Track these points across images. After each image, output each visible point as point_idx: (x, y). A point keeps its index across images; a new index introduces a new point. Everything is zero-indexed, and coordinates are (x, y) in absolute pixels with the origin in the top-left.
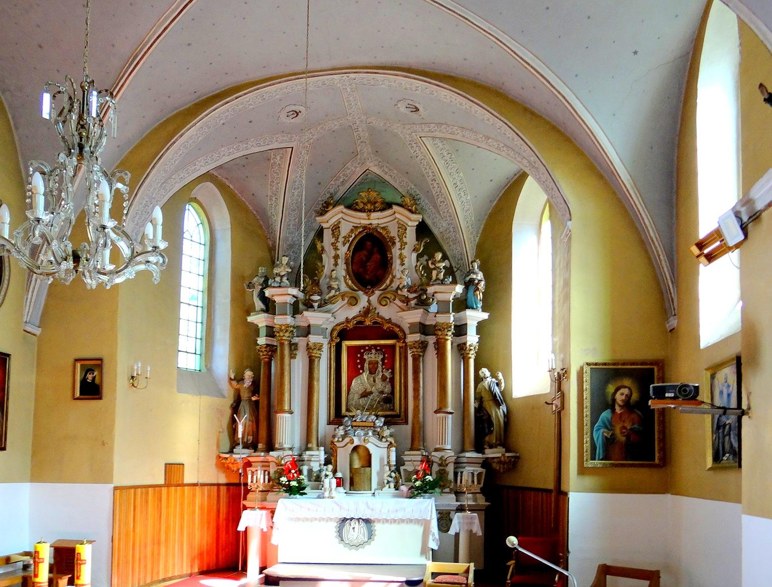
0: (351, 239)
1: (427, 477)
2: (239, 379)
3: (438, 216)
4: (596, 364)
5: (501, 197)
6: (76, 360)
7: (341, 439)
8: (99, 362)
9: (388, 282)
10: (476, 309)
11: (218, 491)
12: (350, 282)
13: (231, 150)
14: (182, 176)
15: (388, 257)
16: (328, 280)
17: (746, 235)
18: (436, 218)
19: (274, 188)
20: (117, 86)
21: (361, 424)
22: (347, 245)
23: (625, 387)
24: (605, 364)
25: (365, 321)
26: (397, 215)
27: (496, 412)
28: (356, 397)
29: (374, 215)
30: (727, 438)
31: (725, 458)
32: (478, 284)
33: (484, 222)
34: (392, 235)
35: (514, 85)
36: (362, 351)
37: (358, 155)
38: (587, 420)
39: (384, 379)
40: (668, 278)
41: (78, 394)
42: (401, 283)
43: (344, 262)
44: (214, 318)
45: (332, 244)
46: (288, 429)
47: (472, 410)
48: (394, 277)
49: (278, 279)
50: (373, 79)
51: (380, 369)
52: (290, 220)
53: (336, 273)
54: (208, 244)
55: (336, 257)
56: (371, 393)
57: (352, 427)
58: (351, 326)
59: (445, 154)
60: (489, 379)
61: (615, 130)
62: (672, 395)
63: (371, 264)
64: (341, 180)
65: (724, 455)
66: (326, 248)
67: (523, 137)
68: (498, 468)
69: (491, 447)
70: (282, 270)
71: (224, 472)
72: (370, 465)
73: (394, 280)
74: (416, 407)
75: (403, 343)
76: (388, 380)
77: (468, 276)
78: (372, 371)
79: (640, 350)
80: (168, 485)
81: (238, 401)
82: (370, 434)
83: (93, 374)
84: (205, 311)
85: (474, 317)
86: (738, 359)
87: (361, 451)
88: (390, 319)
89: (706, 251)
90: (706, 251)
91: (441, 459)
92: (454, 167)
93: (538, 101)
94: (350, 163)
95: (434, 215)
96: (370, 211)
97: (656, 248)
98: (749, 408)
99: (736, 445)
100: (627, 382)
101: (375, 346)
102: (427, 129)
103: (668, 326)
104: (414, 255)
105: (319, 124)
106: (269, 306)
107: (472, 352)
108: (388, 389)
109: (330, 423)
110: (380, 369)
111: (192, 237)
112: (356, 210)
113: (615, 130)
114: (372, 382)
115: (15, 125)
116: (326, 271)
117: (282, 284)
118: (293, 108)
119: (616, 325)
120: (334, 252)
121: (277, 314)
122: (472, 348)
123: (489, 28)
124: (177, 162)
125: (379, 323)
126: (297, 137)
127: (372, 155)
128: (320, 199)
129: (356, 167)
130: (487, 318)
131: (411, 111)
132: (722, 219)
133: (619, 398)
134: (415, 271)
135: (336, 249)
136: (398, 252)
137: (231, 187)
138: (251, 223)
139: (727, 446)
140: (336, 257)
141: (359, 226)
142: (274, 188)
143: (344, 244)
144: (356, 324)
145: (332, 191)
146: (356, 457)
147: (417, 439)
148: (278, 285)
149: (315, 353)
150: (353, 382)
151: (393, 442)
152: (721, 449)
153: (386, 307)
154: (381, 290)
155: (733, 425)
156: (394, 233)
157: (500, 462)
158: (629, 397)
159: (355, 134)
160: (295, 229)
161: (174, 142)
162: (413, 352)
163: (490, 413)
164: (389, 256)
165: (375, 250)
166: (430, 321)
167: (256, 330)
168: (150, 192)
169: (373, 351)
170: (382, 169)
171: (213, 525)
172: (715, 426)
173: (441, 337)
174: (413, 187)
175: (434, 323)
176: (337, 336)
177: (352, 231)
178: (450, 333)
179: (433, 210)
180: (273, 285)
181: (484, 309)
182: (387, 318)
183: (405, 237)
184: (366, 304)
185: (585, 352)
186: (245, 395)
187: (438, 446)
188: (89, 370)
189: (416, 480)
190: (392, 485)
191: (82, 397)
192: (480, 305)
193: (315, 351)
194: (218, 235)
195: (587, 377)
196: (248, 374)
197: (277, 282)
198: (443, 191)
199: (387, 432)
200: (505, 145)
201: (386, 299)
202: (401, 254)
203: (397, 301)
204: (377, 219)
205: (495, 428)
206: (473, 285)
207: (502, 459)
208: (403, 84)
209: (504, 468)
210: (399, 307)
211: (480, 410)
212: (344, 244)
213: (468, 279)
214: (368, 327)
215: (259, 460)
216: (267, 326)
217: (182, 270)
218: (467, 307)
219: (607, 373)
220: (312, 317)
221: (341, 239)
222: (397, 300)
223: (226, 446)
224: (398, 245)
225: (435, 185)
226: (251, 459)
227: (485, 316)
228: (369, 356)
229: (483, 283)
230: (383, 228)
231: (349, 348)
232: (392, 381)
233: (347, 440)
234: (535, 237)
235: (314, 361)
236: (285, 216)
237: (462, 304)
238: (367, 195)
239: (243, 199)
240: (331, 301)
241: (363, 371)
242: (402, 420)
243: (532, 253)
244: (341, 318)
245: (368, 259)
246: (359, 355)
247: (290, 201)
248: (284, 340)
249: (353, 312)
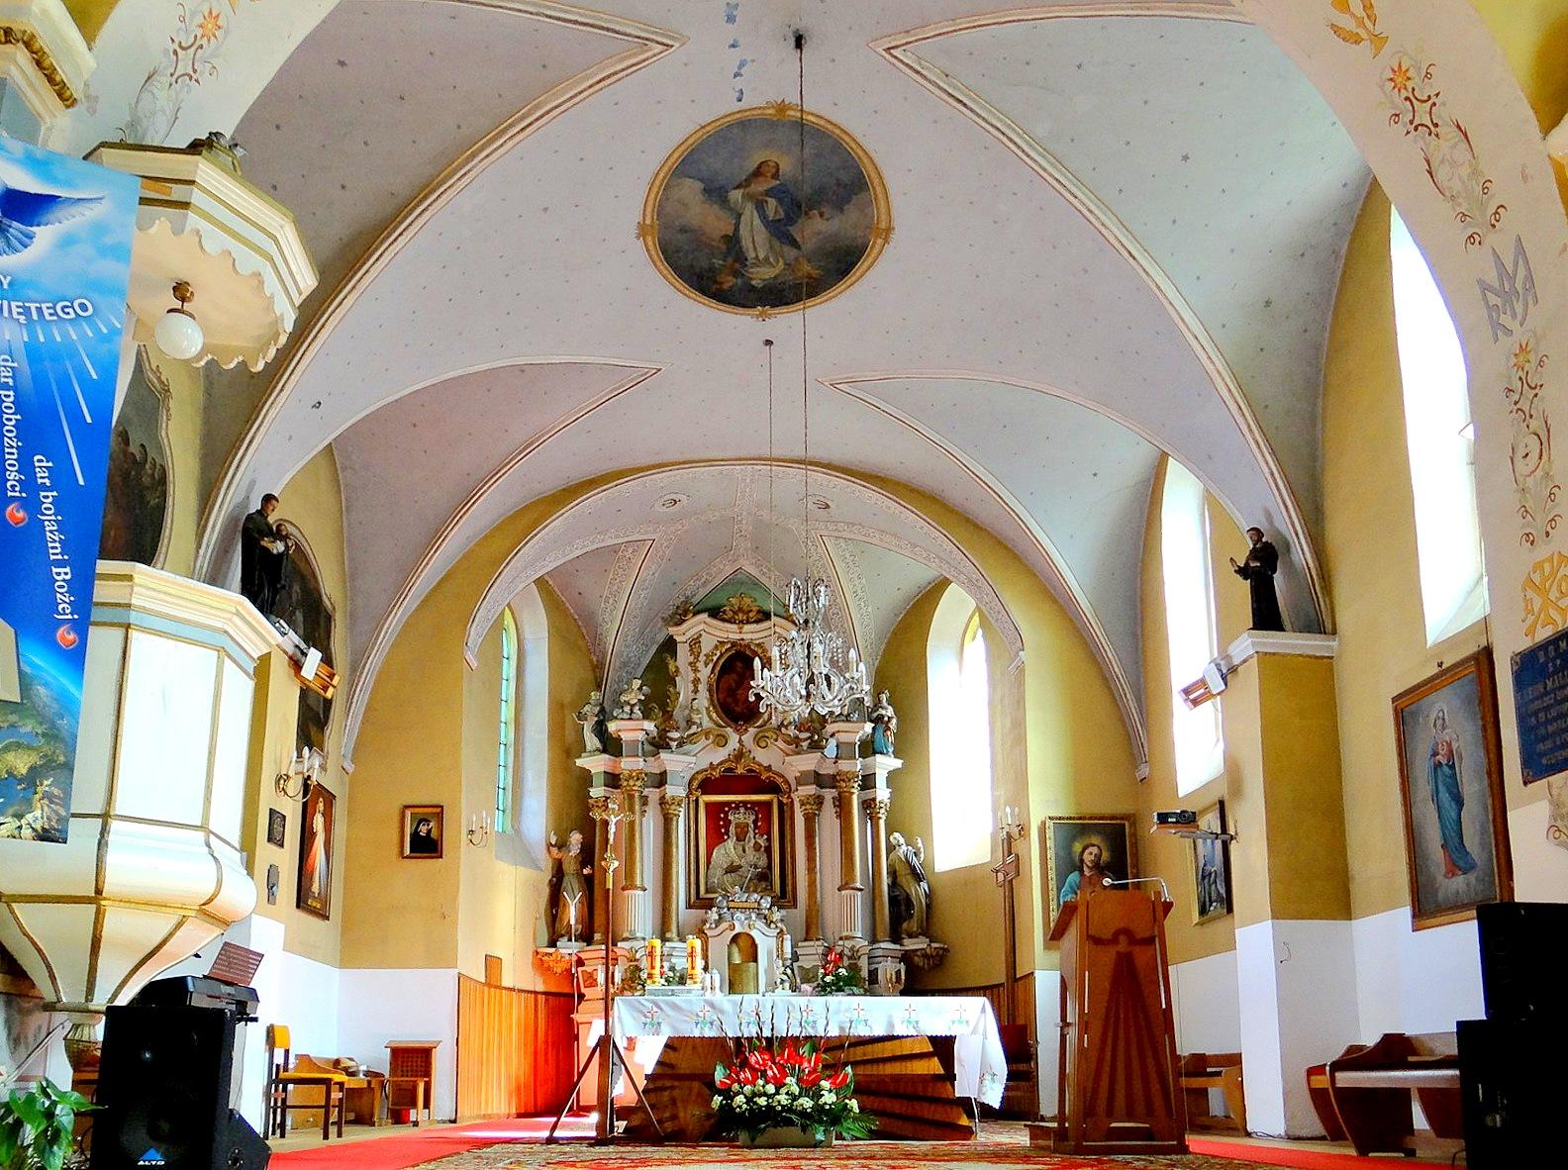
0: (715, 658)
1: (840, 970)
2: (562, 845)
4: (1060, 818)
6: (407, 807)
7: (713, 926)
8: (439, 810)
10: (887, 754)
11: (536, 1000)
12: (714, 715)
16: (687, 712)
17: (1226, 685)
20: (497, 473)
21: (741, 905)
22: (711, 665)
23: (1094, 845)
24: (1070, 818)
26: (778, 630)
27: (916, 890)
28: (719, 872)
29: (747, 628)
30: (1213, 887)
31: (1212, 908)
32: (889, 721)
35: (956, 494)
36: (726, 809)
38: (1052, 885)
39: (757, 848)
40: (1137, 720)
41: (407, 851)
44: (523, 761)
45: (690, 664)
46: (639, 911)
47: (885, 888)
49: (627, 709)
51: (751, 834)
55: (696, 682)
56: (740, 867)
57: (729, 910)
58: (716, 774)
59: (848, 556)
60: (904, 848)
61: (1072, 554)
62: (1174, 820)
64: (703, 580)
65: (1211, 905)
67: (965, 552)
68: (921, 964)
69: (910, 936)
71: (542, 975)
72: (755, 960)
74: (812, 884)
75: (788, 798)
76: (763, 849)
77: (875, 711)
78: (741, 837)
79: (1107, 804)
80: (488, 984)
81: (559, 873)
82: (754, 916)
83: (428, 825)
85: (884, 765)
86: (1222, 803)
87: (742, 942)
88: (770, 766)
89: (1192, 697)
90: (1192, 697)
91: (852, 949)
93: (983, 513)
96: (741, 622)
97: (1122, 685)
98: (1236, 834)
99: (1223, 891)
100: (1096, 840)
101: (745, 803)
103: (1139, 775)
105: (695, 514)
106: (611, 746)
107: (882, 811)
108: (763, 862)
109: (689, 906)
110: (751, 834)
112: (724, 620)
113: (1072, 554)
114: (741, 851)
115: (347, 508)
117: (634, 716)
118: (674, 496)
119: (1079, 777)
122: (882, 805)
123: (940, 440)
125: (755, 771)
128: (671, 603)
130: (900, 766)
132: (1206, 671)
133: (1088, 858)
135: (696, 670)
137: (550, 583)
139: (1214, 897)
140: (696, 682)
143: (706, 665)
144: (723, 772)
145: (688, 593)
146: (735, 950)
147: (811, 929)
148: (628, 716)
149: (672, 810)
150: (715, 851)
151: (785, 929)
152: (1207, 899)
154: (757, 727)
155: (1218, 872)
157: (925, 956)
158: (1098, 857)
162: (806, 809)
163: (908, 891)
166: (828, 769)
167: (586, 778)
169: (742, 810)
171: (531, 1049)
172: (1200, 876)
175: (831, 772)
176: (698, 788)
177: (716, 647)
178: (856, 785)
180: (620, 716)
181: (897, 755)
185: (1046, 801)
186: (570, 867)
187: (844, 934)
188: (424, 820)
189: (826, 975)
190: (787, 985)
191: (412, 855)
192: (891, 750)
193: (673, 807)
194: (528, 646)
195: (1050, 833)
196: (576, 838)
197: (627, 713)
199: (777, 915)
200: (938, 557)
203: (781, 744)
204: (751, 633)
205: (916, 912)
206: (882, 723)
207: (928, 951)
209: (928, 964)
210: (781, 749)
211: (894, 885)
212: (706, 665)
213: (875, 715)
214: (741, 776)
215: (597, 956)
218: (874, 753)
219: (1077, 828)
221: (702, 658)
223: (544, 937)
226: (583, 956)
227: (898, 763)
228: (736, 816)
229: (894, 721)
230: (758, 645)
231: (708, 805)
232: (768, 850)
233: (724, 925)
234: (957, 665)
235: (671, 819)
237: (869, 748)
240: (691, 739)
241: (729, 837)
242: (789, 902)
243: (958, 682)
246: (722, 816)
249: (720, 755)
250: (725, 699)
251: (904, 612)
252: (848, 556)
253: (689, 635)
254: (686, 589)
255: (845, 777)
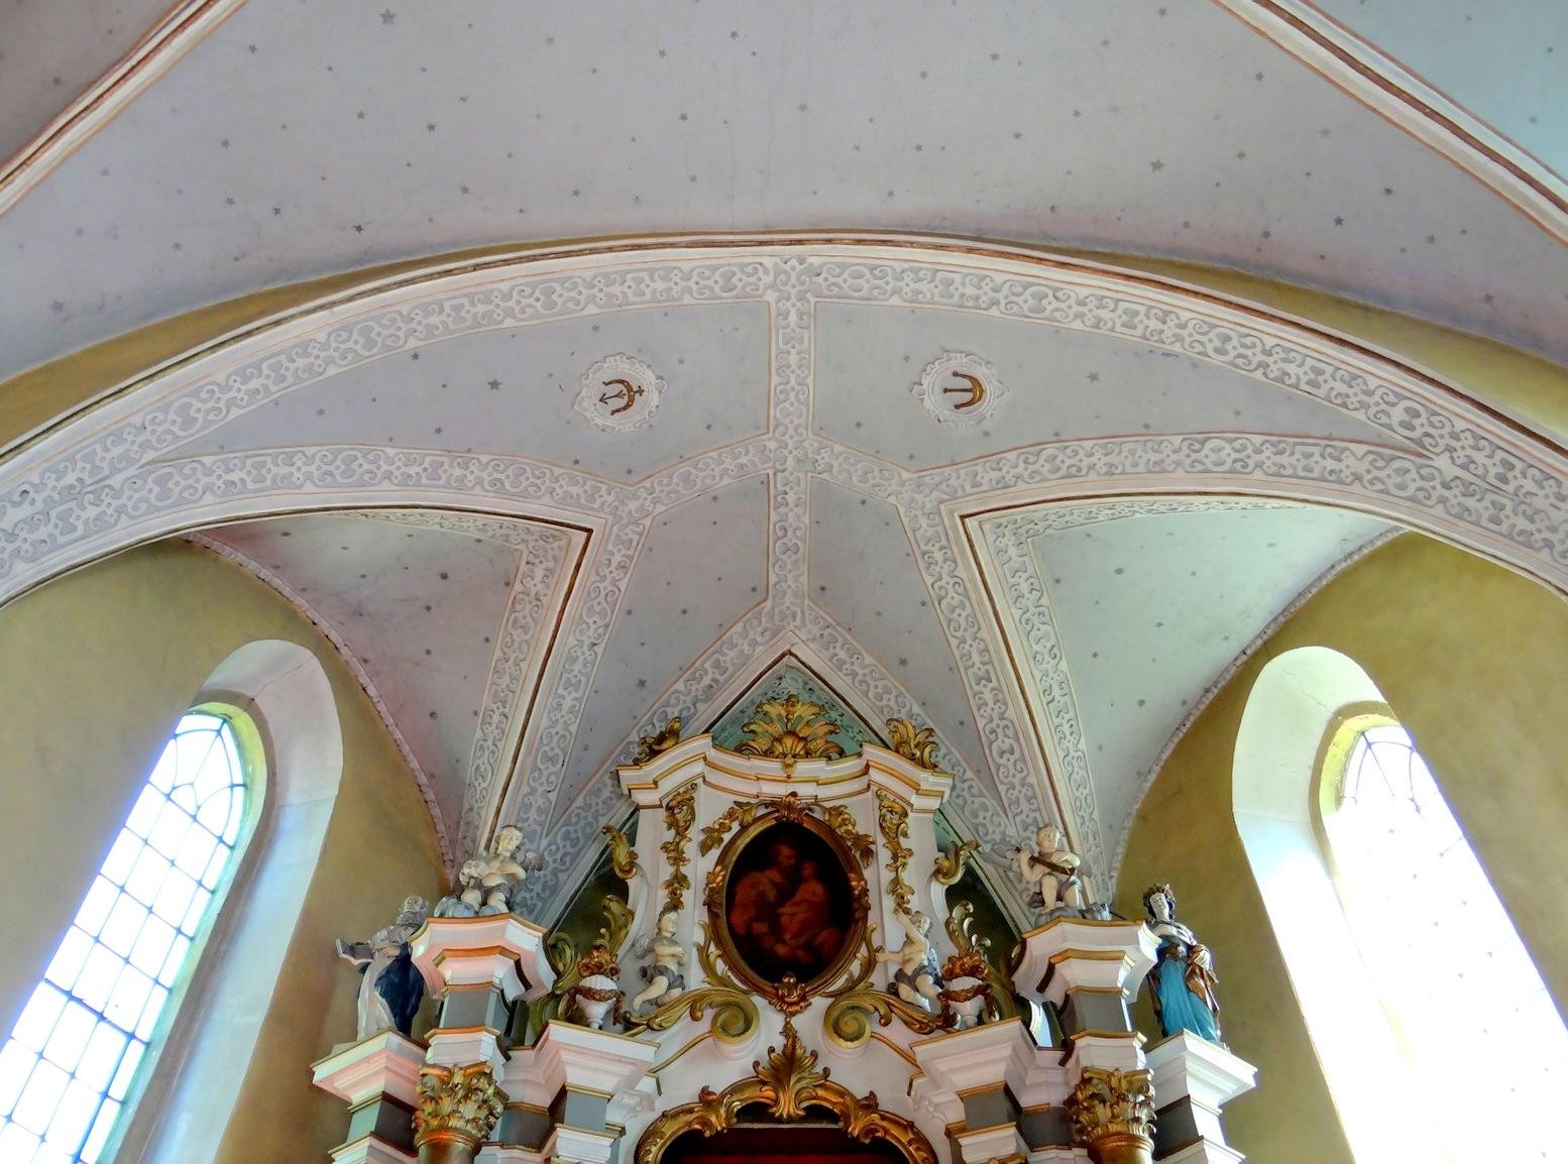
3: (991, 803)
5: (1167, 761)
9: (855, 968)
12: (720, 967)
13: (413, 470)
14: (235, 476)
15: (853, 889)
18: (986, 809)
19: (506, 679)
22: (715, 853)
25: (776, 1102)
29: (803, 768)
33: (1124, 836)
34: (860, 830)
37: (765, 600)
42: (908, 961)
43: (702, 898)
45: (665, 848)
48: (874, 952)
49: (472, 897)
50: (873, 268)
52: (533, 791)
53: (676, 924)
54: (240, 853)
55: (678, 882)
58: (718, 1121)
59: (1024, 587)
63: (796, 909)
64: (707, 681)
66: (643, 860)
70: (493, 871)
73: (880, 957)
84: (156, 1054)
92: (1047, 636)
94: (739, 628)
95: (977, 801)
102: (988, 476)
104: (938, 891)
111: (199, 807)
116: (639, 928)
120: (672, 869)
121: (442, 1025)
124: (235, 412)
125: (830, 1116)
126: (611, 498)
127: (807, 602)
129: (754, 644)
131: (957, 407)
134: (947, 938)
136: (887, 876)
137: (372, 691)
138: (410, 818)
141: (753, 801)
142: (506, 679)
143: (705, 848)
153: (857, 1043)
154: (830, 995)
156: (864, 820)
159: (774, 517)
160: (542, 825)
161: (249, 334)
164: (854, 883)
165: (808, 869)
168: (109, 456)
170: (831, 650)
173: (1113, 1128)
174: (916, 709)
177: (731, 815)
179: (977, 783)
182: (860, 1093)
183: (905, 835)
184: (779, 1042)
194: (289, 820)
197: (468, 907)
198: (1010, 713)
201: (857, 1014)
202: (896, 882)
208: (958, 283)
212: (705, 848)
216: (387, 1098)
217: (124, 826)
220: (582, 1055)
221: (695, 834)
222: (896, 1023)
224: (884, 855)
225: (988, 697)
234: (1310, 859)
236: (521, 773)
238: (785, 714)
239: (398, 735)
244: (682, 1089)
245: (786, 893)
247: (545, 722)
248: (455, 1129)
249: (732, 1065)
250: (748, 926)
251: (1157, 769)
252: (1024, 587)
253: (668, 785)
254: (667, 704)
255: (1105, 1091)
